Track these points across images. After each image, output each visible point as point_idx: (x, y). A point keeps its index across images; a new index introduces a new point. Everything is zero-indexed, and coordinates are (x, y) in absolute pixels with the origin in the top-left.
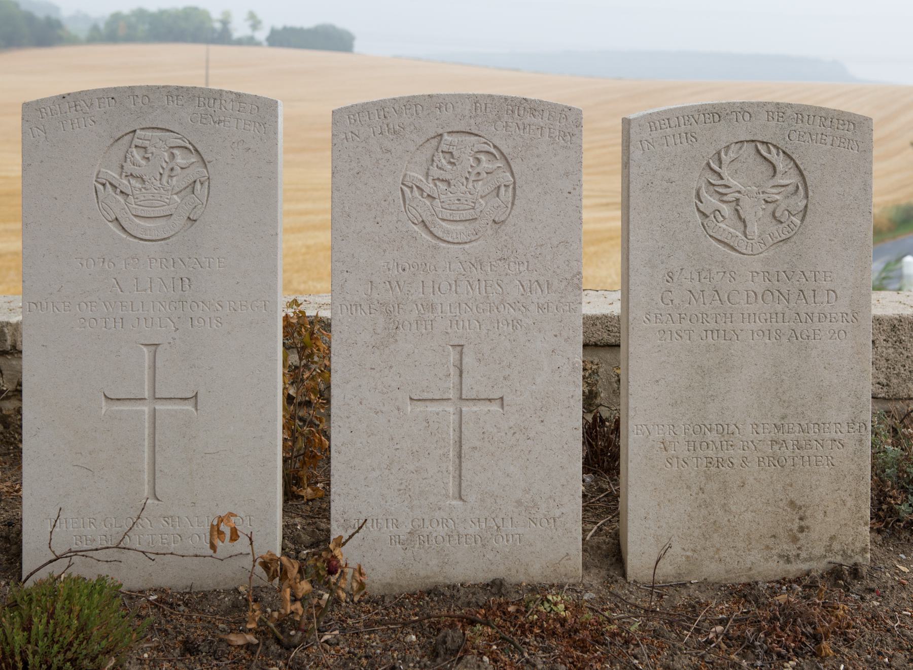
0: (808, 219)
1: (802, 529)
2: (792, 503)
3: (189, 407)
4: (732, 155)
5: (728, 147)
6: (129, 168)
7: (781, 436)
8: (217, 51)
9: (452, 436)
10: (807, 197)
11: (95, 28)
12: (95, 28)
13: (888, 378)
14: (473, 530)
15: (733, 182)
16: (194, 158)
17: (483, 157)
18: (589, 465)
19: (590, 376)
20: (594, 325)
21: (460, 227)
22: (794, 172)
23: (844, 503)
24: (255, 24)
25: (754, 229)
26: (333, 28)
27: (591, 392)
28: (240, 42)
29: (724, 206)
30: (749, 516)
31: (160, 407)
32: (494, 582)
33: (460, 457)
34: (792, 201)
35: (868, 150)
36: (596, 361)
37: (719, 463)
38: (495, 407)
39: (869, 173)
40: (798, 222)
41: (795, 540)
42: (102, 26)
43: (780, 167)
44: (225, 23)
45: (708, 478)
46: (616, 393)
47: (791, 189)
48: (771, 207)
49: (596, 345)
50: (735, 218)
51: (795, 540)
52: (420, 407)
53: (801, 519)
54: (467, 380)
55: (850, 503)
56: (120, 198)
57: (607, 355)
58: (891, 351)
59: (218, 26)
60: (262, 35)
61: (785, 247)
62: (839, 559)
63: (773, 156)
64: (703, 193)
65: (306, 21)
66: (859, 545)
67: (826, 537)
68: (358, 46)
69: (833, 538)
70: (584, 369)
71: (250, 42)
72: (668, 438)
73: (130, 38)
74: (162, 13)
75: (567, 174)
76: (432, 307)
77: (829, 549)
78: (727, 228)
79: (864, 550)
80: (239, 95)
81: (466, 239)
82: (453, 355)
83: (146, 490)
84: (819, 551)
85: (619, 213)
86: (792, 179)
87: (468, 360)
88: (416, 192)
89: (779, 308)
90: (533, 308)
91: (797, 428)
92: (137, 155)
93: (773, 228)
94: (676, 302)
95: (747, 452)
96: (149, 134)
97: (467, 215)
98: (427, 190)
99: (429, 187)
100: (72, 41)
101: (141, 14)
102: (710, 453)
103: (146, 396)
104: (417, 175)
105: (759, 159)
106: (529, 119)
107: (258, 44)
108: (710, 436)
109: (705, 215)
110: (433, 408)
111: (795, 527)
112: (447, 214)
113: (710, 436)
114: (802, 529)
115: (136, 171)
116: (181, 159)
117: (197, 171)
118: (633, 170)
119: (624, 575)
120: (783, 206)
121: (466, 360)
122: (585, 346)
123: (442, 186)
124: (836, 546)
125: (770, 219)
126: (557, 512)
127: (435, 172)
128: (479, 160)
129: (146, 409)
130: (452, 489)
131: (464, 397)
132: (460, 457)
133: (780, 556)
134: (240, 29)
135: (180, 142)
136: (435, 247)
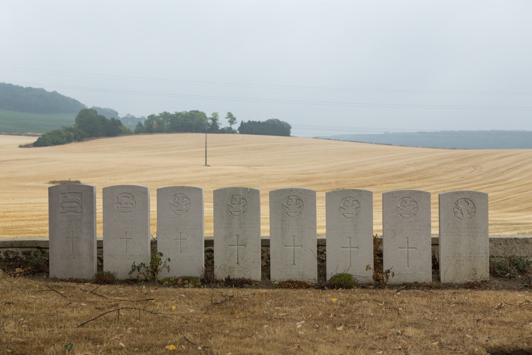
0: (475, 213)
1: (475, 274)
2: (473, 268)
3: (357, 249)
4: (460, 201)
5: (459, 199)
6: (232, 202)
7: (471, 255)
8: (211, 136)
9: (407, 255)
10: (475, 209)
11: (140, 124)
12: (140, 124)
13: (504, 252)
14: (411, 273)
15: (460, 206)
16: (357, 203)
17: (411, 202)
18: (433, 268)
19: (433, 252)
20: (434, 240)
21: (407, 215)
22: (472, 204)
23: (484, 269)
24: (232, 119)
25: (465, 215)
26: (278, 121)
27: (433, 255)
28: (223, 131)
29: (459, 211)
30: (465, 271)
31: (352, 249)
32: (415, 282)
33: (408, 259)
34: (472, 210)
35: (487, 200)
36: (435, 248)
37: (459, 261)
38: (415, 249)
39: (488, 204)
40: (473, 214)
41: (474, 276)
42: (143, 123)
43: (470, 203)
44: (214, 120)
45: (456, 263)
46: (439, 256)
47: (472, 207)
48: (468, 211)
49: (435, 244)
50: (461, 213)
51: (474, 276)
52: (400, 249)
53: (475, 272)
54: (409, 244)
55: (485, 269)
56: (344, 210)
57: (436, 246)
58: (505, 246)
59: (210, 121)
60: (236, 127)
61: (471, 219)
62: (483, 279)
63: (468, 201)
64: (455, 208)
65: (263, 118)
66: (487, 277)
67: (480, 275)
68: (293, 132)
69: (482, 275)
70: (432, 250)
71: (229, 131)
72: (448, 256)
73: (160, 130)
74: (178, 114)
75: (428, 205)
76: (402, 230)
77: (481, 277)
78: (459, 215)
79: (488, 278)
80: (365, 191)
81: (408, 217)
82: (406, 240)
83: (349, 264)
84: (479, 278)
85: (438, 210)
86: (472, 205)
87: (409, 240)
88: (399, 209)
89: (470, 231)
90: (422, 230)
91: (474, 254)
92: (347, 202)
93: (468, 215)
94: (450, 229)
95: (464, 259)
96: (349, 198)
97: (408, 213)
98: (401, 208)
99: (401, 208)
100: (127, 133)
101: (166, 115)
102: (457, 259)
103: (349, 247)
104: (399, 205)
105: (465, 202)
106: (420, 195)
107: (234, 132)
108: (457, 255)
109: (455, 213)
110: (403, 249)
111: (474, 273)
112: (405, 213)
113: (457, 255)
114: (475, 274)
115: (347, 205)
116: (185, 199)
117: (358, 205)
118: (441, 204)
119: (440, 282)
120: (470, 211)
121: (409, 240)
122: (432, 245)
123: (404, 207)
124: (482, 277)
125: (468, 213)
126: (427, 270)
127: (403, 205)
128: (411, 203)
129: (349, 249)
130: (406, 265)
131: (409, 247)
132: (408, 259)
133: (471, 279)
134: (223, 123)
135: (355, 200)
136: (403, 219)
